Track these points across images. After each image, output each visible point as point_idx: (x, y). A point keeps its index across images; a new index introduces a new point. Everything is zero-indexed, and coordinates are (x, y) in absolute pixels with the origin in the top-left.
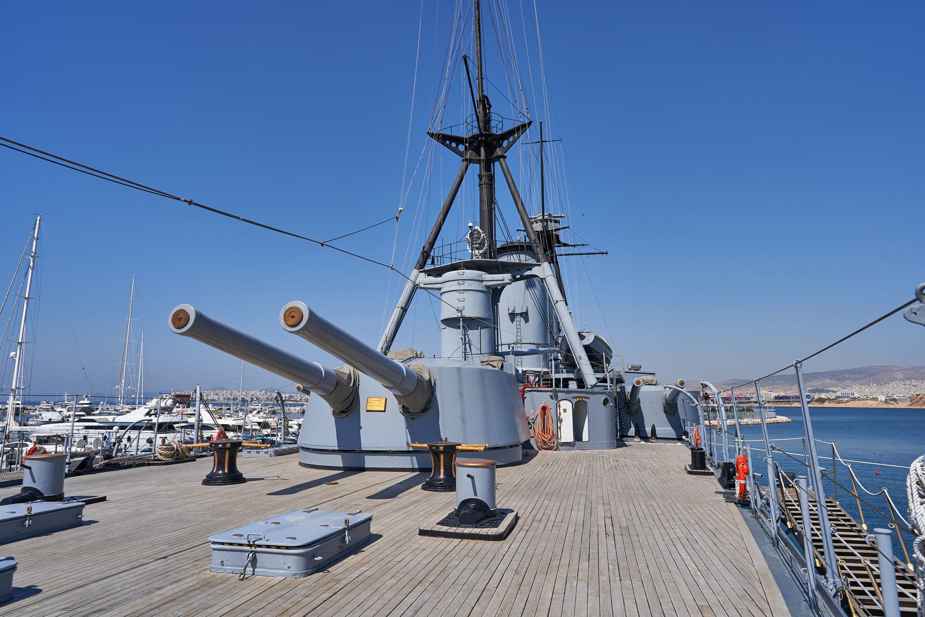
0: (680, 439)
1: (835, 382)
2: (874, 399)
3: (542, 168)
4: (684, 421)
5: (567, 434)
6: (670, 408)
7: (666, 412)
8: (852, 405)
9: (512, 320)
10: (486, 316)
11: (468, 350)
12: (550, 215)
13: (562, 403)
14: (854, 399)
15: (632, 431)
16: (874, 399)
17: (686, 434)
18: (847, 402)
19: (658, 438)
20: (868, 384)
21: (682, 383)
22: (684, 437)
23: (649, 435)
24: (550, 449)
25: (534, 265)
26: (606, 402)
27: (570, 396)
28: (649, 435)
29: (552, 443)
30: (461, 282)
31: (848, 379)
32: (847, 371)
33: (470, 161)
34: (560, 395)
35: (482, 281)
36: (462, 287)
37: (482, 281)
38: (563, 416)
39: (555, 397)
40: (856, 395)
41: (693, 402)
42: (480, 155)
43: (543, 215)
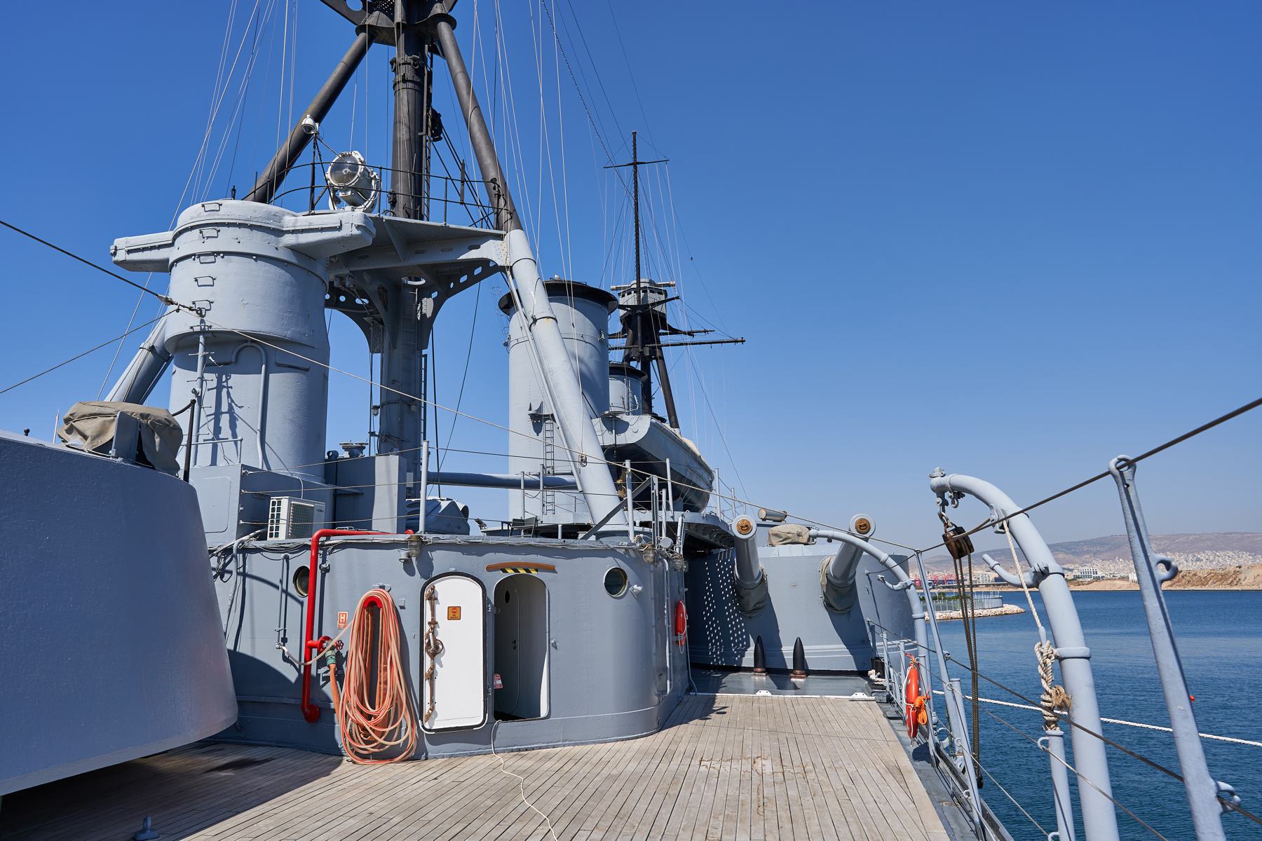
0: (863, 674)
1: (1071, 557)
2: (1122, 578)
3: (636, 204)
4: (872, 628)
5: (459, 693)
6: (840, 596)
7: (828, 606)
8: (1096, 587)
9: (538, 429)
10: (288, 334)
11: (226, 432)
12: (651, 282)
13: (441, 586)
14: (1097, 579)
15: (748, 659)
16: (1122, 578)
17: (879, 666)
18: (1090, 583)
19: (808, 673)
20: (1112, 559)
21: (863, 527)
22: (873, 674)
23: (790, 666)
24: (386, 756)
25: (486, 237)
26: (615, 582)
27: (476, 563)
28: (790, 666)
29: (405, 738)
30: (208, 232)
31: (1087, 552)
32: (1085, 542)
33: (374, 35)
34: (440, 559)
35: (279, 233)
36: (211, 246)
37: (279, 233)
38: (447, 631)
39: (421, 564)
40: (1100, 574)
41: (896, 579)
42: (392, 18)
43: (638, 283)
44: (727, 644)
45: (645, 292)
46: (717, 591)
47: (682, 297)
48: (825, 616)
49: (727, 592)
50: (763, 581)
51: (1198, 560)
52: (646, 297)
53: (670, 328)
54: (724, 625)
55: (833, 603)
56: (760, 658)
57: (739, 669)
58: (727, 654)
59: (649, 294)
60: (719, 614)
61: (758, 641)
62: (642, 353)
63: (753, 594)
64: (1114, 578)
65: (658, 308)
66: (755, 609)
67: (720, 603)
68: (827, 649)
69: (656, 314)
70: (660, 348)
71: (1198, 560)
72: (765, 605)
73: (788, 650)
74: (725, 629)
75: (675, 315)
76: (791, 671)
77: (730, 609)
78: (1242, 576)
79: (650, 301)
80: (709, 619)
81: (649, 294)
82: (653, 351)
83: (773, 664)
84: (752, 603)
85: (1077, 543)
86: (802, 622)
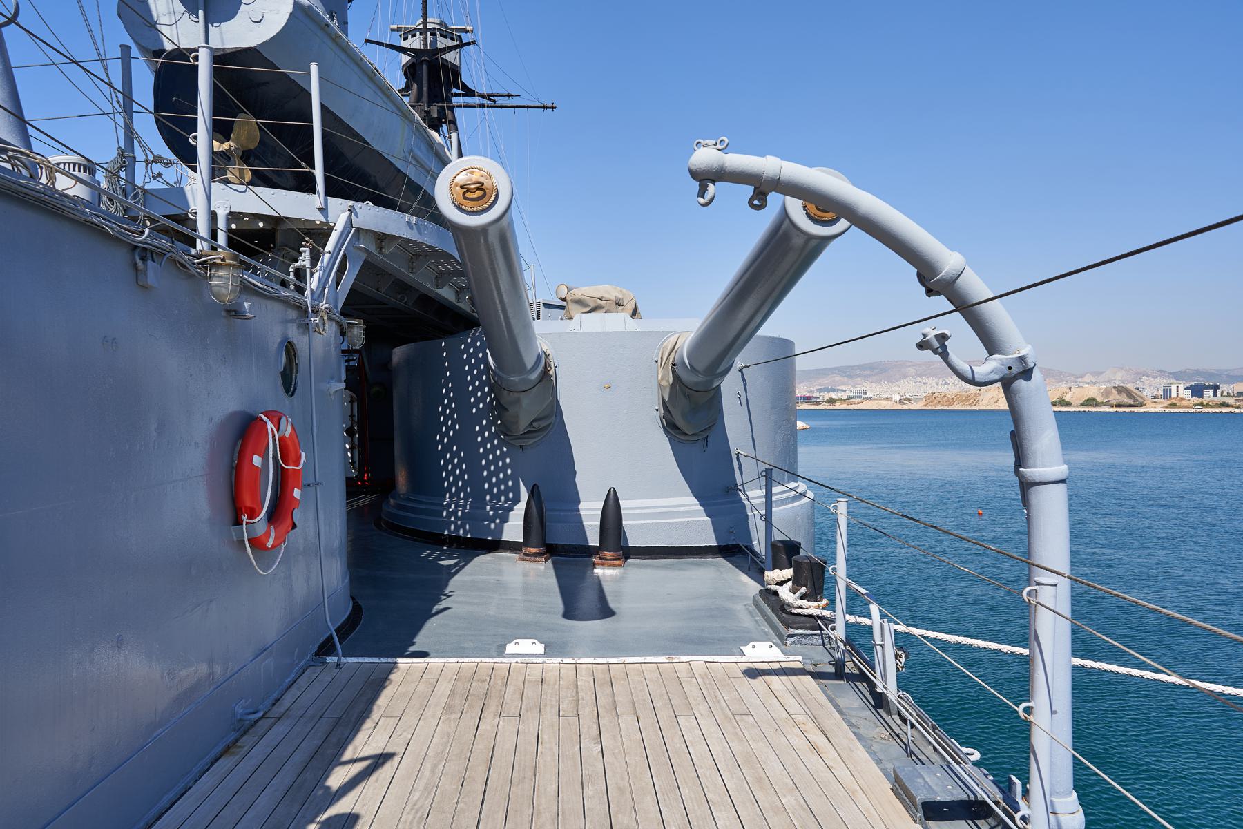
7: (671, 427)
14: (867, 399)
15: (513, 529)
19: (628, 553)
20: (879, 382)
23: (594, 540)
28: (594, 540)
31: (859, 376)
40: (869, 395)
43: (425, 22)
44: (478, 498)
45: (433, 34)
46: (462, 396)
47: (480, 42)
48: (662, 443)
49: (480, 399)
50: (546, 377)
51: (946, 384)
52: (434, 42)
53: (465, 87)
54: (473, 460)
55: (680, 422)
56: (536, 523)
57: (495, 545)
58: (477, 516)
59: (439, 38)
60: (465, 439)
61: (534, 492)
62: (428, 113)
63: (525, 401)
64: (880, 399)
65: (450, 57)
66: (530, 432)
67: (468, 421)
68: (664, 507)
69: (446, 64)
70: (451, 109)
71: (946, 384)
72: (550, 424)
73: (590, 511)
74: (475, 469)
75: (474, 69)
76: (595, 550)
77: (484, 431)
78: (980, 398)
79: (440, 46)
80: (447, 448)
81: (439, 38)
82: (442, 111)
83: (559, 535)
84: (531, 424)
85: (852, 367)
86: (621, 462)
